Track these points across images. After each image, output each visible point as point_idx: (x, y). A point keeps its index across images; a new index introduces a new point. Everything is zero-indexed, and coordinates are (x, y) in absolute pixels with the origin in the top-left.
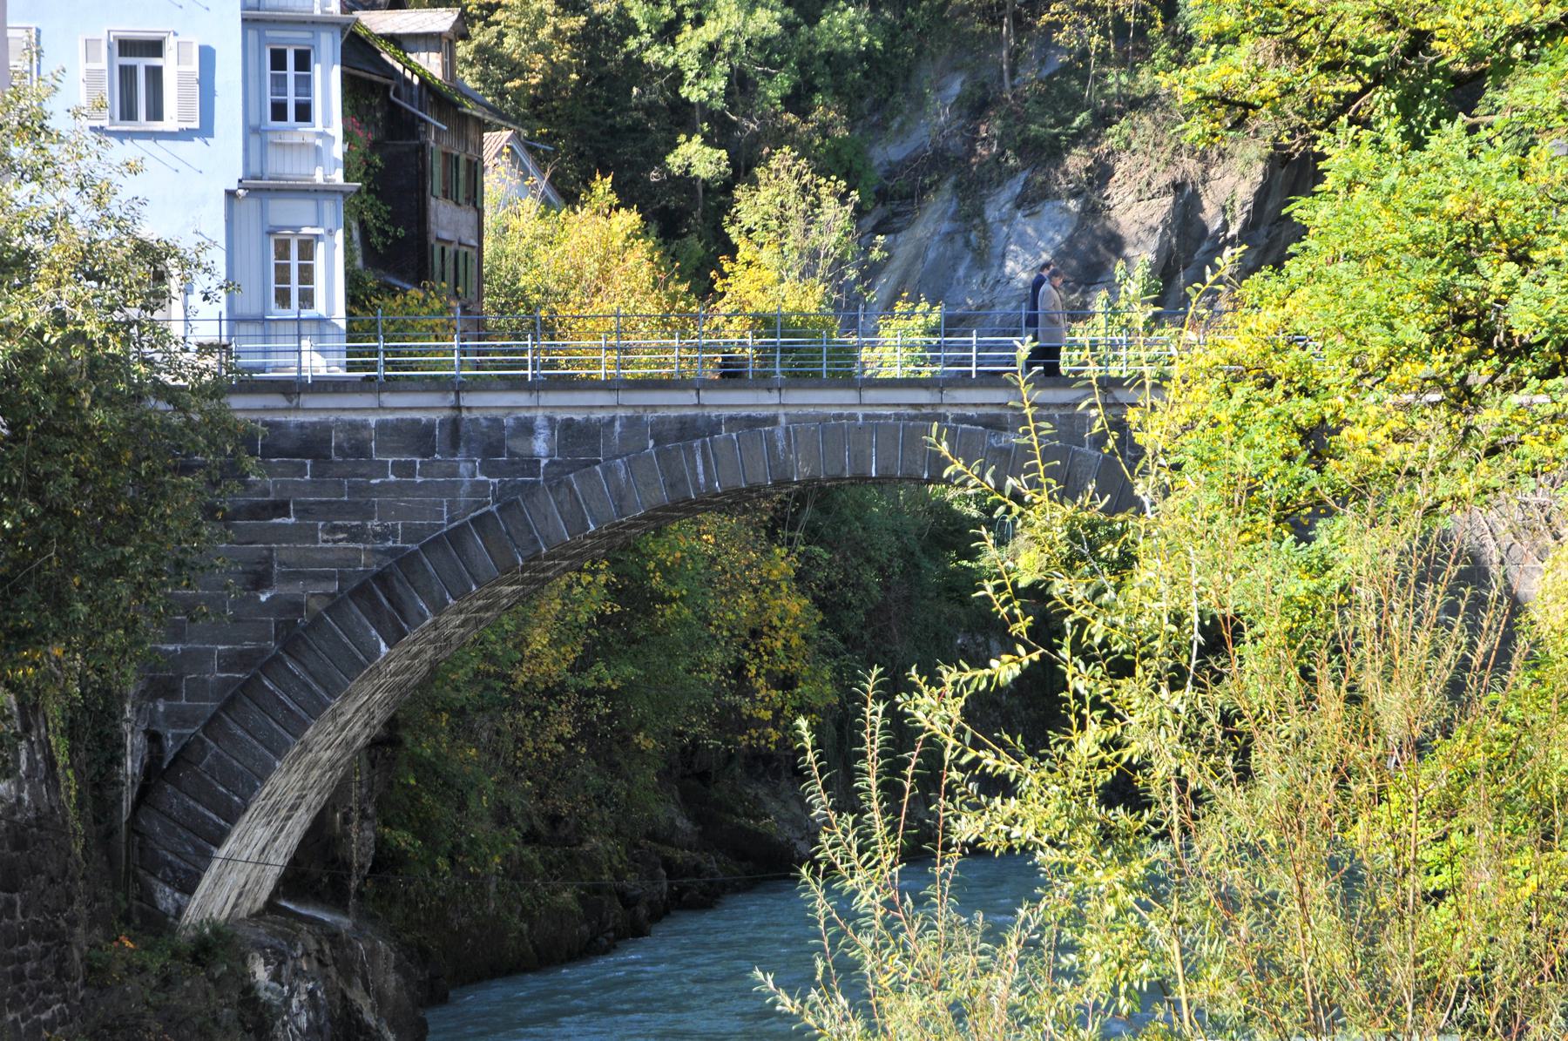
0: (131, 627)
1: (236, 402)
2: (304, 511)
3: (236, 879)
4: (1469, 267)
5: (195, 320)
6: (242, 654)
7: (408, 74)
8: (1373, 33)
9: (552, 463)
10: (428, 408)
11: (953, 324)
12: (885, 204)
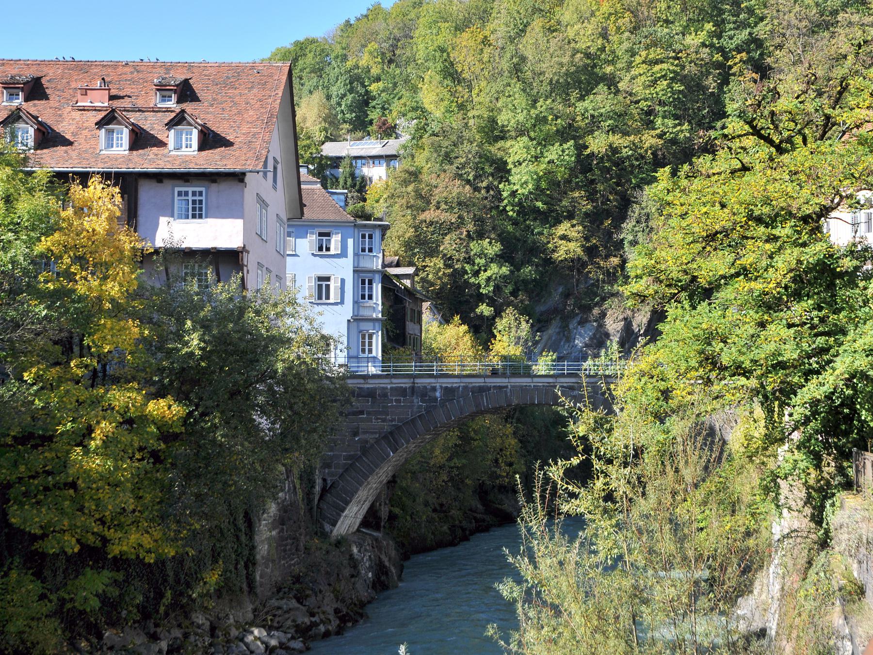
0: (318, 447)
1: (349, 381)
2: (369, 413)
3: (348, 522)
4: (709, 344)
5: (338, 358)
8: (681, 276)
10: (405, 383)
11: (560, 359)
12: (539, 324)
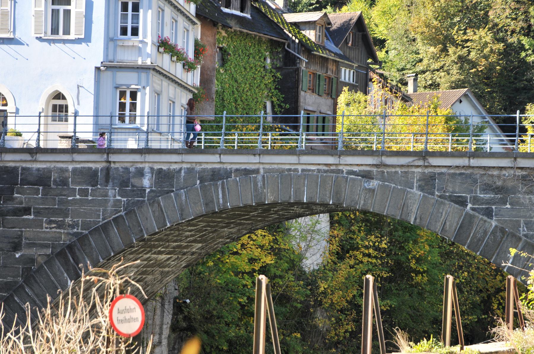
2: (38, 213)
6: (6, 283)
7: (294, 38)
9: (151, 191)
